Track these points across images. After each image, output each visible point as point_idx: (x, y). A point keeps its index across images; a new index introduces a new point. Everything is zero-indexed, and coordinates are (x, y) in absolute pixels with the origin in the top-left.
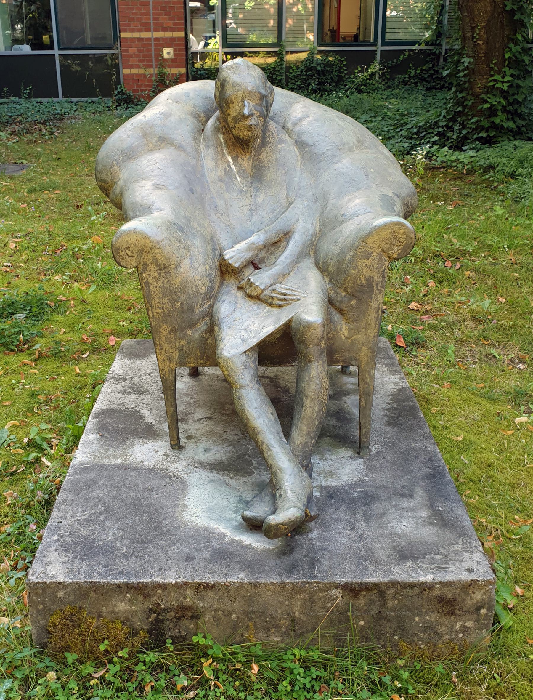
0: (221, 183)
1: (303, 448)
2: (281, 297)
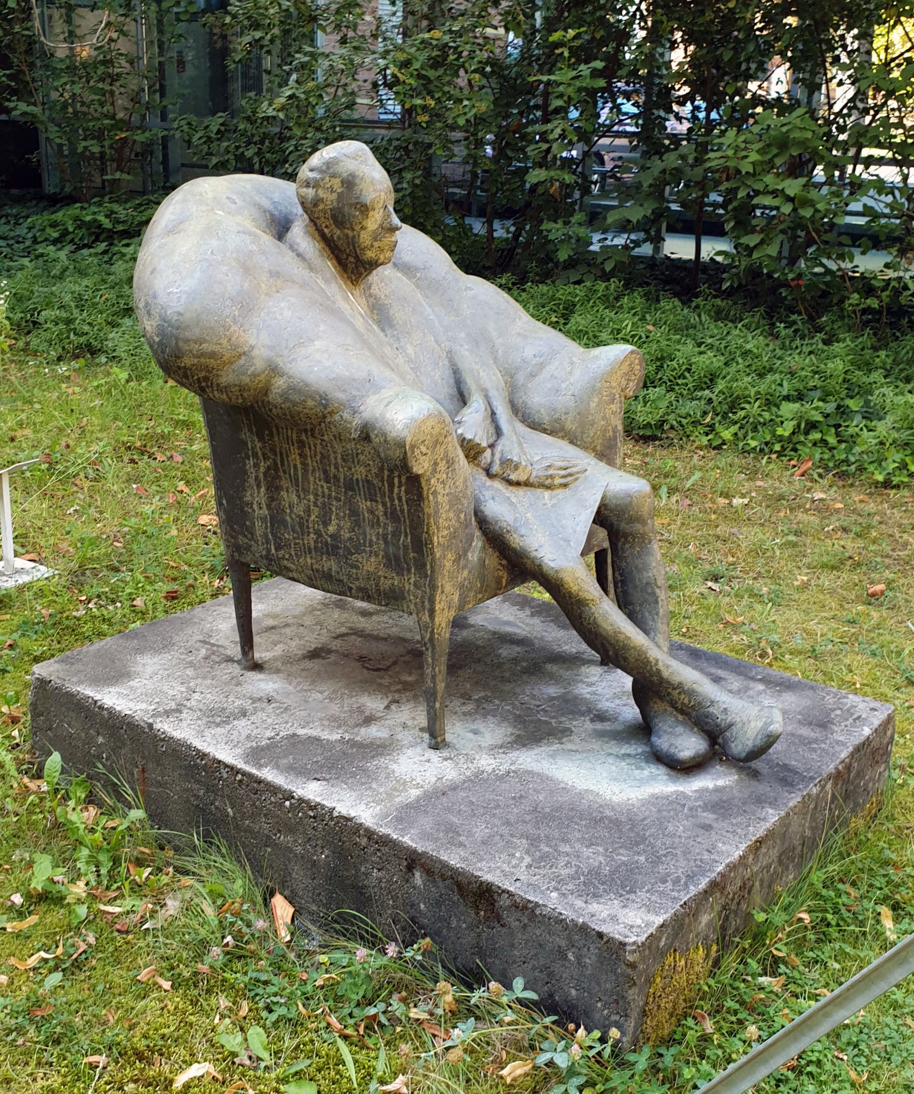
2: (563, 472)
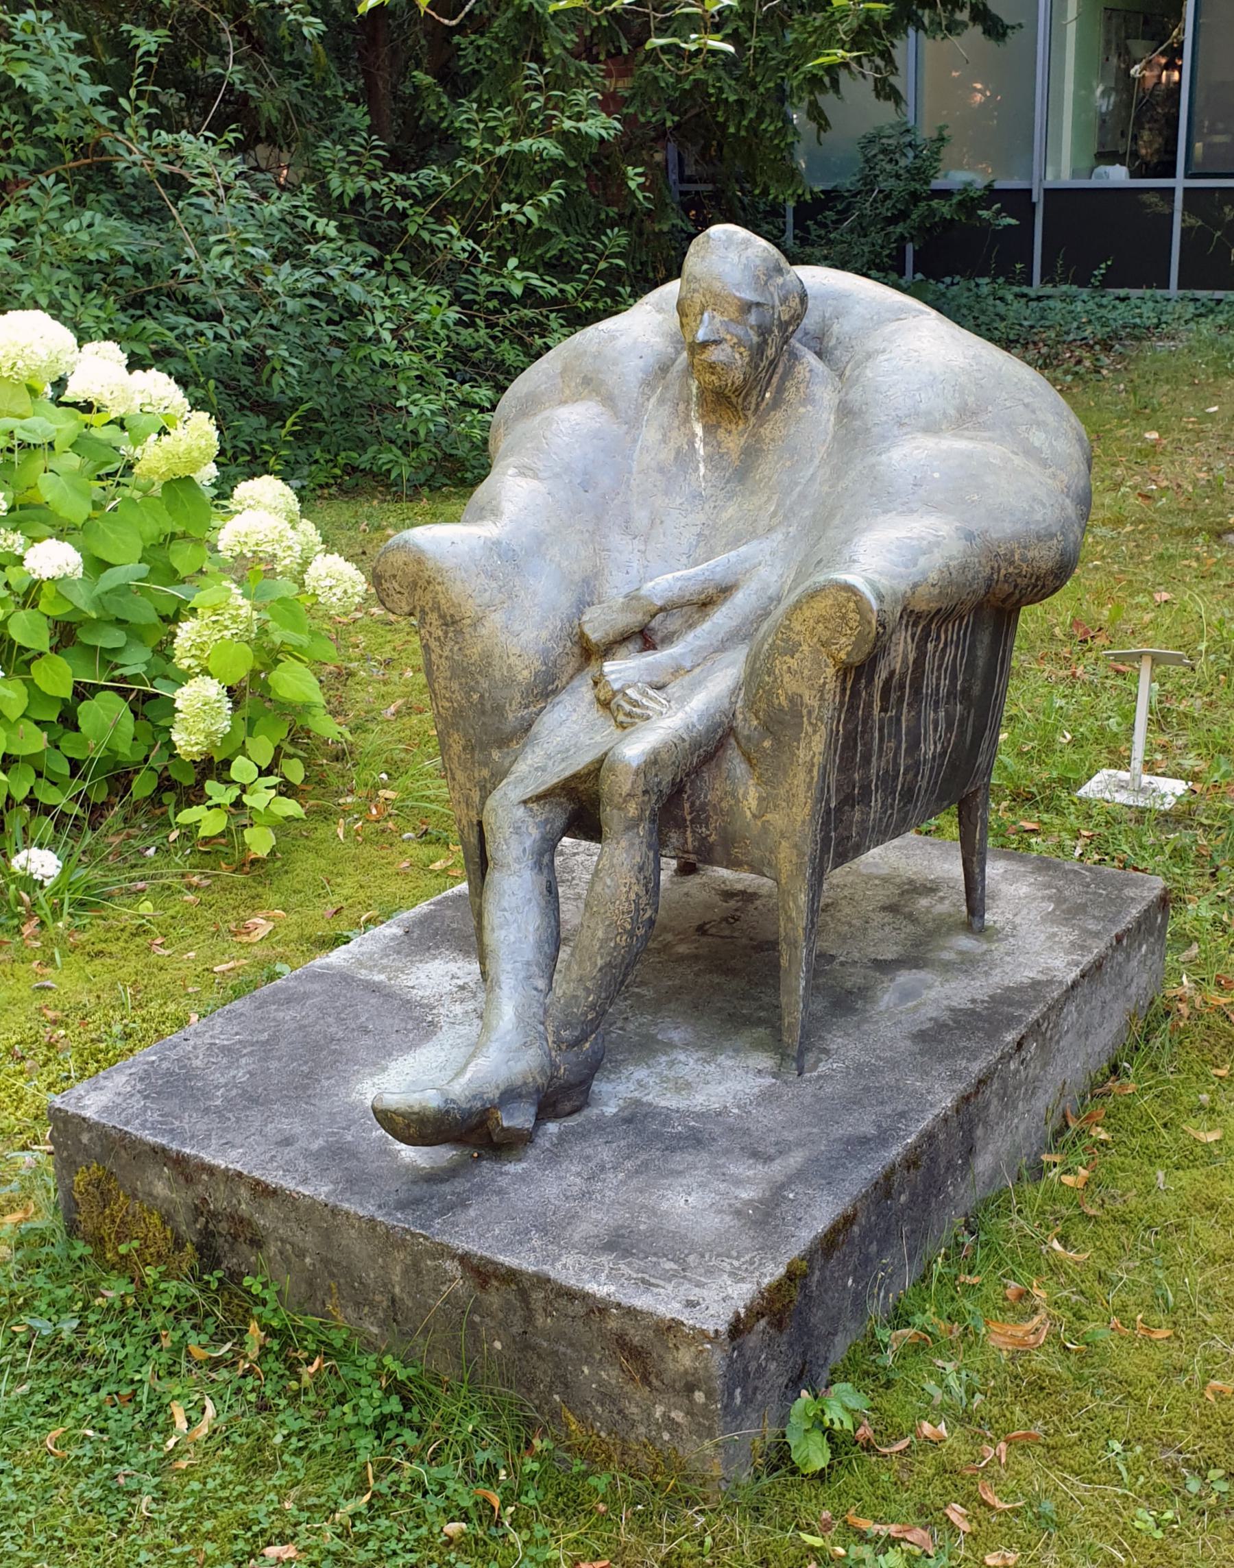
0: (659, 476)
1: (567, 1005)
